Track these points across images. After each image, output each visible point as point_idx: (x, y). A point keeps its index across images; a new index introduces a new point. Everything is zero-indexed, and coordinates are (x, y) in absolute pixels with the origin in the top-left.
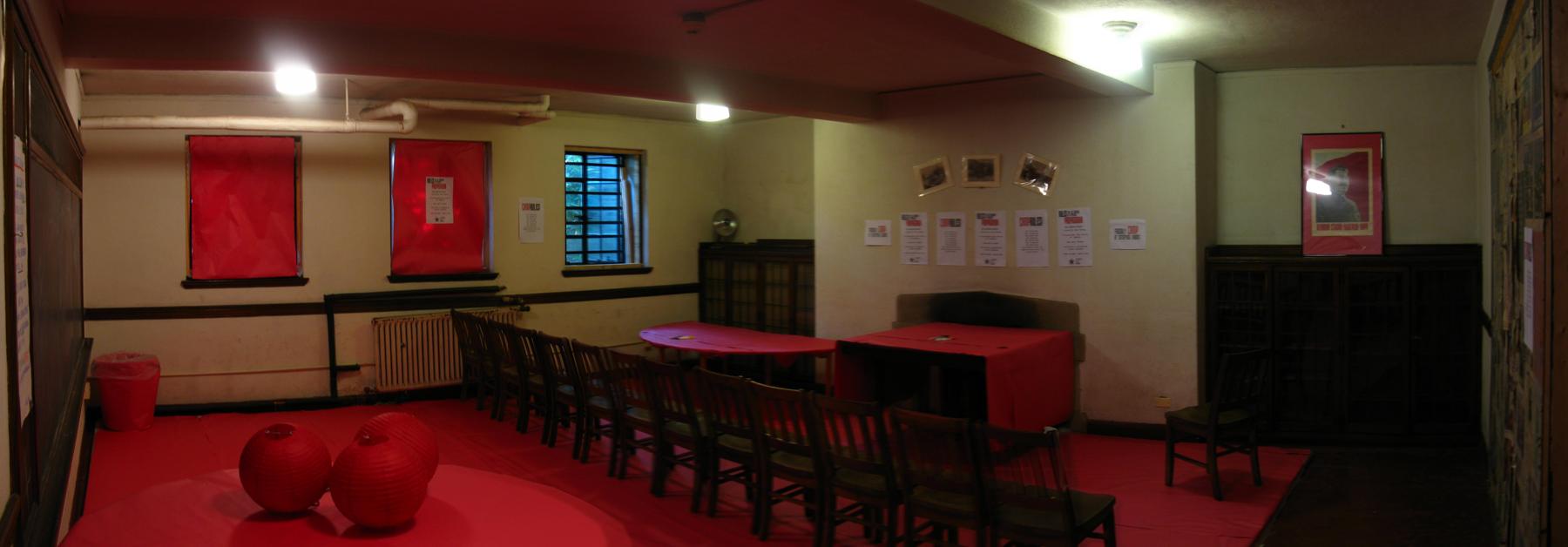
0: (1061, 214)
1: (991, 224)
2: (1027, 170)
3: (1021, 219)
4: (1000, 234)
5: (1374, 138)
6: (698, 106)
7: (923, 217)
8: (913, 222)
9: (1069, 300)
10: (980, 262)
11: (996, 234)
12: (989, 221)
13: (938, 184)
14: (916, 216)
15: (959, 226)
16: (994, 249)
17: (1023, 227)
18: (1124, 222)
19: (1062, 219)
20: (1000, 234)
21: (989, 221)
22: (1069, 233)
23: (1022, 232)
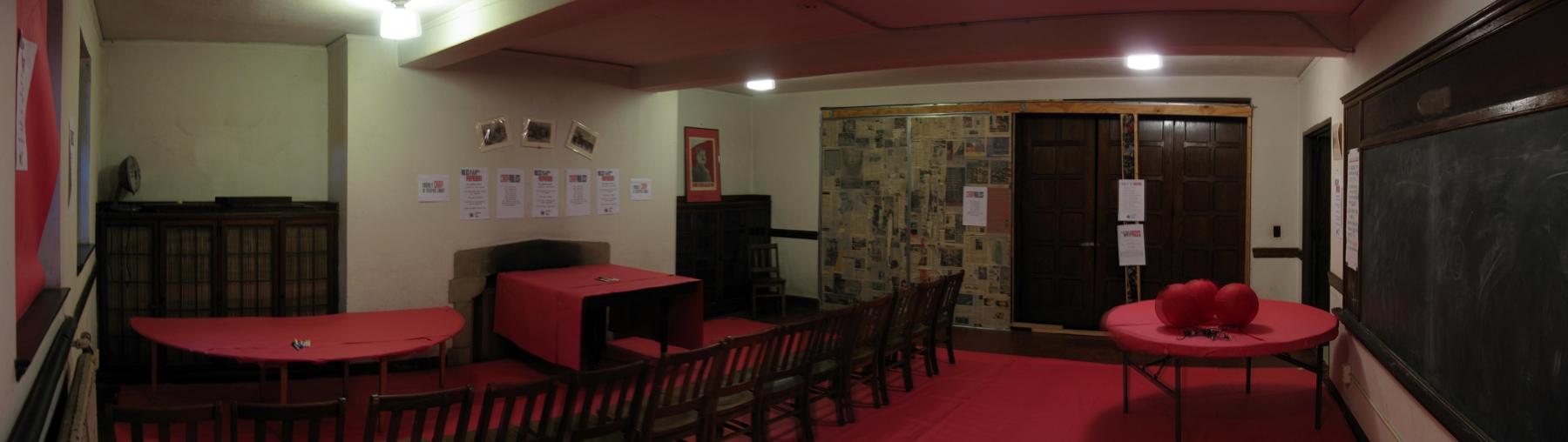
0: (599, 173)
1: (546, 180)
2: (577, 136)
3: (570, 176)
4: (482, 189)
5: (714, 133)
6: (1125, 58)
7: (484, 174)
8: (473, 176)
9: (597, 239)
10: (536, 213)
11: (550, 189)
12: (545, 177)
13: (500, 141)
14: (477, 171)
15: (518, 181)
16: (478, 203)
17: (504, 183)
18: (638, 181)
19: (537, 177)
20: (482, 189)
21: (545, 177)
22: (542, 189)
23: (571, 186)
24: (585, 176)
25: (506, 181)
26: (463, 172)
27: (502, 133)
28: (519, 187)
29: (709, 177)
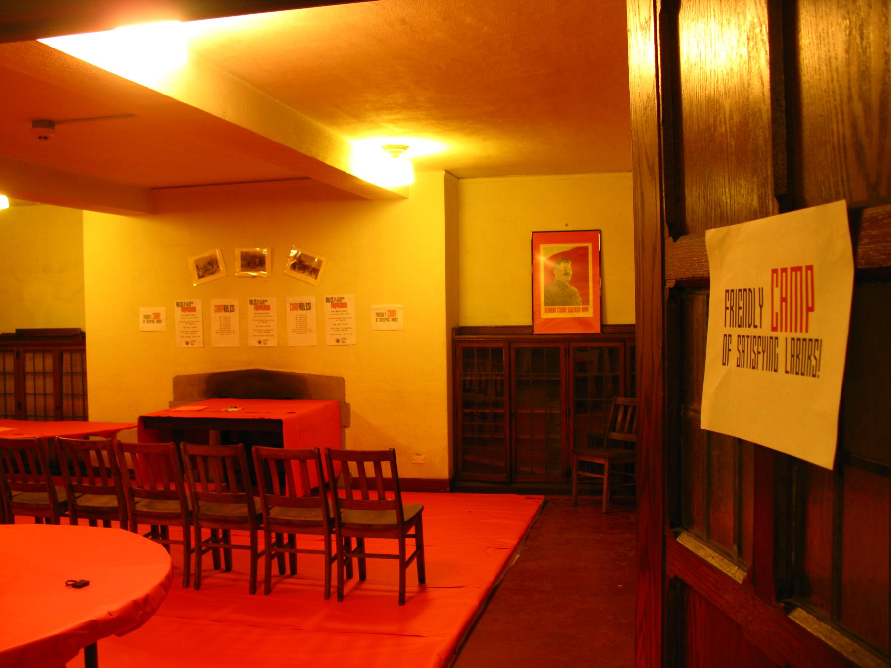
5: (593, 235)
7: (198, 306)
8: (187, 308)
12: (261, 306)
13: (213, 273)
16: (268, 331)
18: (384, 307)
19: (329, 304)
21: (261, 306)
24: (232, 306)
25: (296, 309)
26: (178, 304)
27: (215, 266)
28: (234, 317)
29: (579, 299)
